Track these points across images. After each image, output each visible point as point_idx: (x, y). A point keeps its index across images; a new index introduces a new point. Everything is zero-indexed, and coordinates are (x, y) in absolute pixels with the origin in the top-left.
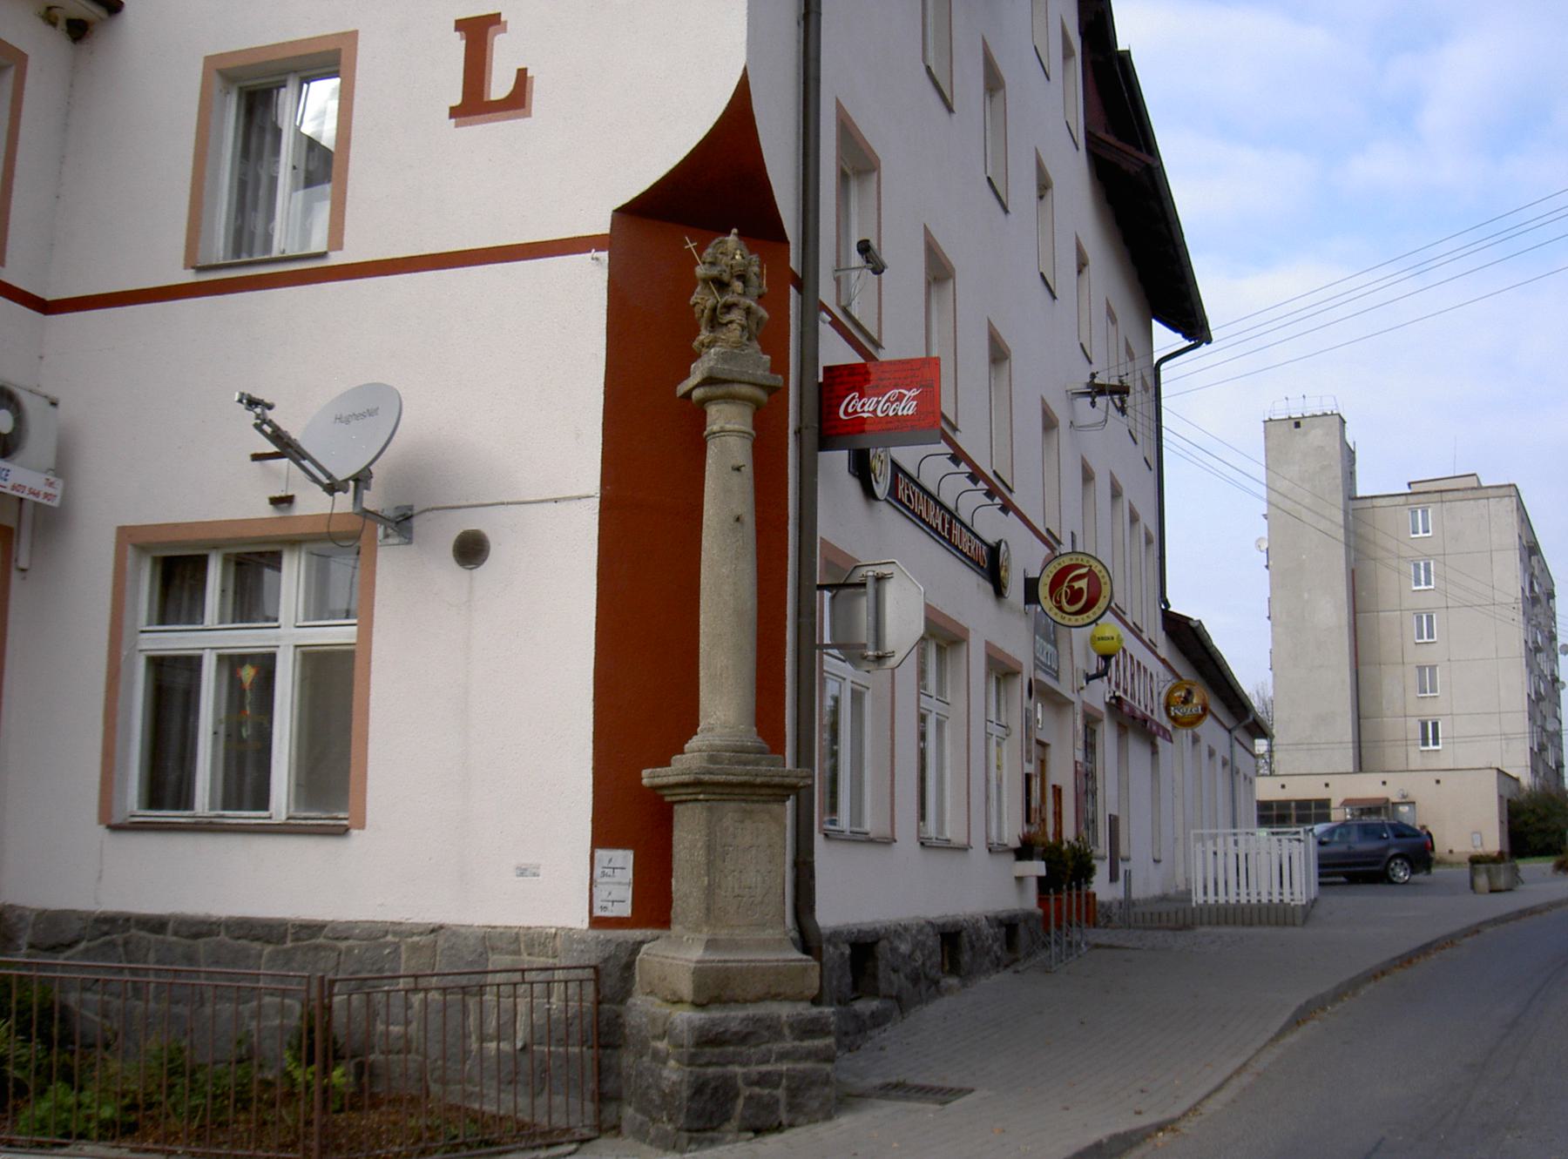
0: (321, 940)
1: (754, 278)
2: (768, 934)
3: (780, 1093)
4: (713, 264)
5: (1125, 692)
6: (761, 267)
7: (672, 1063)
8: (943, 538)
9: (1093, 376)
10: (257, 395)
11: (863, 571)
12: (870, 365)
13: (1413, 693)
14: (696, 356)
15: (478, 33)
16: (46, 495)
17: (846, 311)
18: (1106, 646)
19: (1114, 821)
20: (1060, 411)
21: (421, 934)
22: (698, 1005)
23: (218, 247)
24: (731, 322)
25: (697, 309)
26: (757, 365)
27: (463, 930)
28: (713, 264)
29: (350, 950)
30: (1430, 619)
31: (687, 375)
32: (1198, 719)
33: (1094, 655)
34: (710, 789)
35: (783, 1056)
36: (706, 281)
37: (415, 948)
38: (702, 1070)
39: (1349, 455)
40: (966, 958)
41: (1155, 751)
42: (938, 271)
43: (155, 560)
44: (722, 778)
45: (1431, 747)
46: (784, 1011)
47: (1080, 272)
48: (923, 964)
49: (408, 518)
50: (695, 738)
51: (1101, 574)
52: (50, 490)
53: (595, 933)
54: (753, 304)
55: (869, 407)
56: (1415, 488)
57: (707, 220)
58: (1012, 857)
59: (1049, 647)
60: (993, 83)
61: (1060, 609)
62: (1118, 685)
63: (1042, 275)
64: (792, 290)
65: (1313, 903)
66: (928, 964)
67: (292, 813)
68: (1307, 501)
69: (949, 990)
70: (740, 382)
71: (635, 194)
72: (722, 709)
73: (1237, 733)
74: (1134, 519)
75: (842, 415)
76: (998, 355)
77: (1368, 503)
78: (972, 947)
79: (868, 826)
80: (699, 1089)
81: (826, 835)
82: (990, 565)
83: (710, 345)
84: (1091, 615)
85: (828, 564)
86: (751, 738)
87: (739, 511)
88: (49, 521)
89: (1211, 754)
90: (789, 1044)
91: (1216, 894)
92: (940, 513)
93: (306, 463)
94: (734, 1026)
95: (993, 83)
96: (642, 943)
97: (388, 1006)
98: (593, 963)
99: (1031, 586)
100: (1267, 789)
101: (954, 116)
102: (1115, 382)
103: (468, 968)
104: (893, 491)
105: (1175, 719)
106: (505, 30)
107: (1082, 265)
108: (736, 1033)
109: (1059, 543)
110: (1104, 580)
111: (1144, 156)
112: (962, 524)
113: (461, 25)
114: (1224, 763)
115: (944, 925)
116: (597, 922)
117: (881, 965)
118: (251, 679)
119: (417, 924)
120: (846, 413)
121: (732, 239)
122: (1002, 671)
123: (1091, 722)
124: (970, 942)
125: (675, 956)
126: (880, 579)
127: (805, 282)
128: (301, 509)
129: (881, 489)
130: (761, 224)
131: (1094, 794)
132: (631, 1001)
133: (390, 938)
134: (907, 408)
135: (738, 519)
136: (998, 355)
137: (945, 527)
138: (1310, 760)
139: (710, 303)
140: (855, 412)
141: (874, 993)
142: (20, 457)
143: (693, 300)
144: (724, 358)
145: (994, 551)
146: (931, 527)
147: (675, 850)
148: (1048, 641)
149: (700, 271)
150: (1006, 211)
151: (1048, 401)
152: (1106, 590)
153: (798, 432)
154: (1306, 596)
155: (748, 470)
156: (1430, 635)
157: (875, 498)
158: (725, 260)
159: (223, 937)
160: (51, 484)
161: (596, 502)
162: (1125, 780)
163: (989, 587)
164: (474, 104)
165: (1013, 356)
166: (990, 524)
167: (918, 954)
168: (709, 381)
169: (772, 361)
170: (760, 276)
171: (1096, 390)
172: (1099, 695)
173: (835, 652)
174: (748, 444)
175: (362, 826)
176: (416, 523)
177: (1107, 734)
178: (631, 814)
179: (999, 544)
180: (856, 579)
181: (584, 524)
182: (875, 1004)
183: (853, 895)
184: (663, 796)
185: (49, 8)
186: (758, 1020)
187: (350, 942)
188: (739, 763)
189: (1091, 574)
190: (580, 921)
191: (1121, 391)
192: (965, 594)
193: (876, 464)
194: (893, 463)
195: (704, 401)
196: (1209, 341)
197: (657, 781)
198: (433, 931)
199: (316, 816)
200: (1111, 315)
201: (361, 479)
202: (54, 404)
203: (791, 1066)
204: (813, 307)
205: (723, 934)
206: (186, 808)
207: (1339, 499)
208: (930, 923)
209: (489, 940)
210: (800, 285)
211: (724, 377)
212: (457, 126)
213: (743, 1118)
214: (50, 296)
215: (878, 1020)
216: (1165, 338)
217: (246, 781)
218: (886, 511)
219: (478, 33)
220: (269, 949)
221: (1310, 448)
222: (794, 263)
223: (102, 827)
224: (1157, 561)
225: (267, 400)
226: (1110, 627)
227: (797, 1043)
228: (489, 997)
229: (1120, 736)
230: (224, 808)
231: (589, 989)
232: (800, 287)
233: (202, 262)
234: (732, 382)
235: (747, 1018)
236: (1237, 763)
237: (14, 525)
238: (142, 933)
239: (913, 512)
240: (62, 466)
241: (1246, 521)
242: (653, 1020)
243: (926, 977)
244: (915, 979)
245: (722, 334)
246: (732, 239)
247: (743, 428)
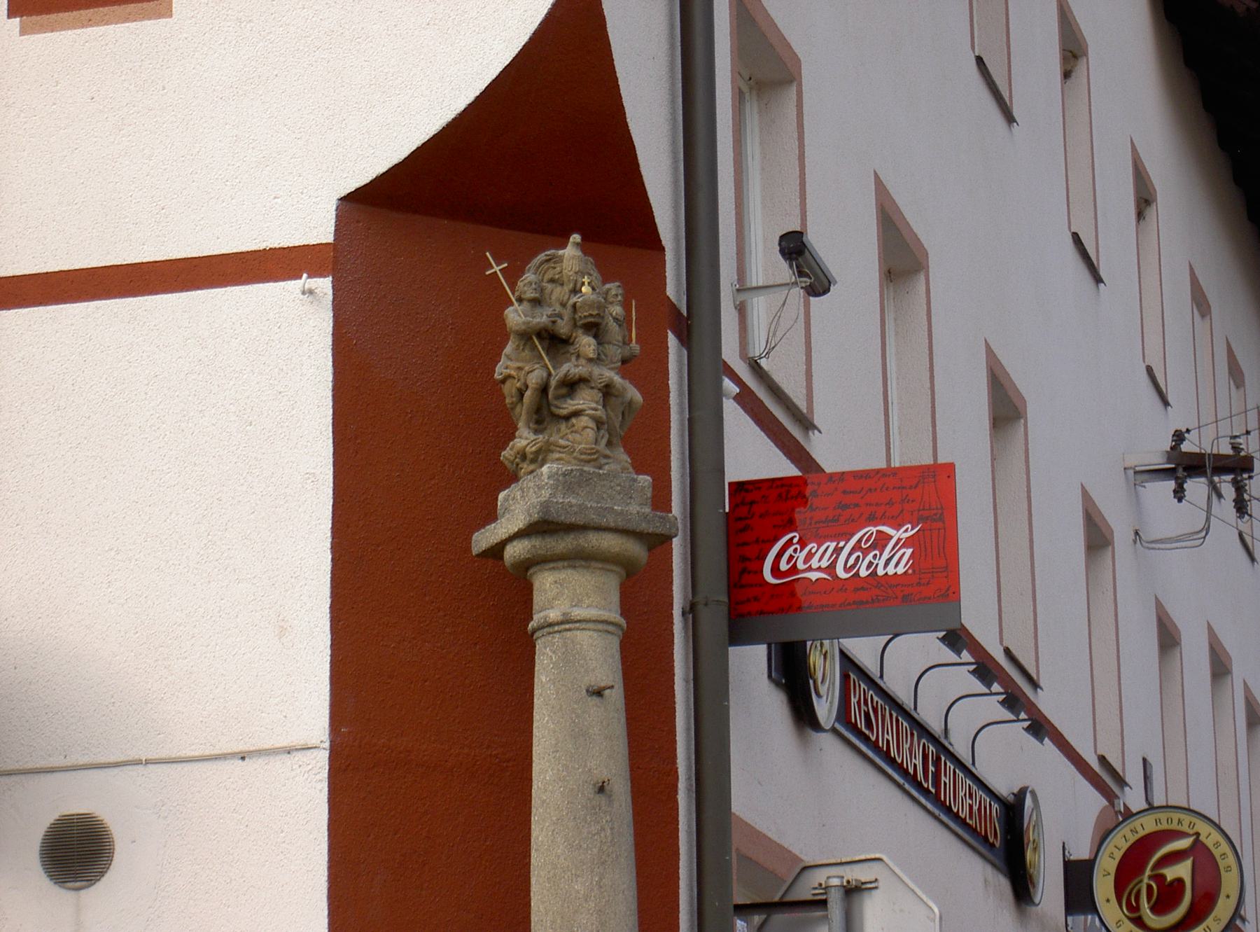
1: (613, 326)
4: (537, 302)
6: (626, 306)
8: (926, 792)
9: (1179, 437)
11: (820, 877)
12: (811, 478)
14: (511, 478)
17: (755, 367)
24: (577, 414)
25: (509, 389)
26: (623, 495)
28: (537, 302)
31: (490, 515)
36: (526, 336)
42: (901, 260)
47: (1140, 215)
51: (1220, 849)
54: (617, 379)
55: (814, 560)
63: (1076, 238)
64: (672, 340)
70: (599, 529)
71: (382, 168)
83: (539, 457)
87: (602, 773)
92: (919, 744)
99: (1078, 877)
102: (1226, 449)
104: (844, 713)
107: (1144, 202)
109: (1121, 782)
110: (1226, 861)
120: (775, 571)
121: (571, 253)
126: (852, 891)
127: (694, 325)
129: (825, 709)
130: (618, 222)
134: (895, 562)
135: (601, 790)
139: (535, 378)
143: (500, 370)
144: (567, 483)
146: (903, 771)
149: (516, 316)
150: (1010, 118)
151: (1094, 495)
152: (1229, 883)
153: (691, 610)
155: (616, 696)
157: (815, 725)
158: (558, 293)
161: (321, 759)
163: (1004, 884)
165: (1032, 411)
166: (1005, 758)
168: (541, 527)
170: (624, 322)
171: (1184, 466)
174: (615, 643)
179: (1021, 795)
180: (804, 891)
181: (300, 801)
189: (1199, 850)
191: (1237, 466)
193: (815, 659)
195: (527, 565)
200: (1200, 302)
204: (706, 371)
210: (685, 329)
212: (23, 32)
218: (828, 747)
222: (674, 288)
232: (685, 339)
239: (875, 746)
245: (560, 435)
246: (571, 253)
247: (605, 615)
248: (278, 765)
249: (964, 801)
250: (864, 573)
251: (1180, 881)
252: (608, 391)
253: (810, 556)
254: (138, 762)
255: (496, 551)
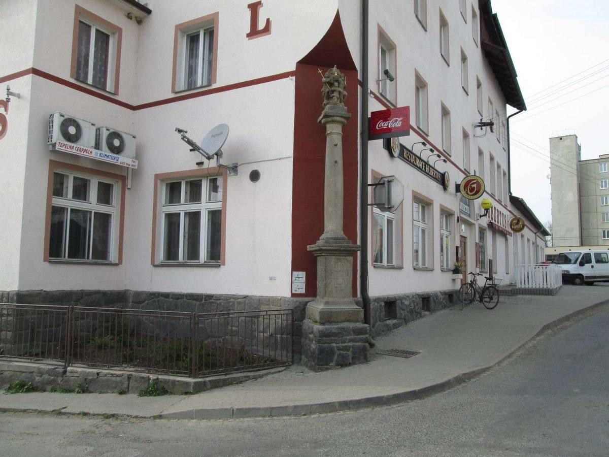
0: (212, 300)
2: (346, 300)
3: (350, 353)
4: (328, 77)
5: (495, 221)
7: (314, 342)
8: (423, 171)
9: (481, 120)
10: (181, 128)
13: (600, 222)
15: (254, 8)
16: (132, 165)
17: (381, 94)
18: (486, 206)
19: (490, 261)
20: (470, 132)
21: (241, 298)
22: (322, 324)
23: (182, 84)
24: (333, 96)
25: (323, 94)
27: (253, 297)
29: (221, 303)
30: (606, 198)
32: (521, 229)
33: (483, 210)
34: (325, 252)
35: (351, 341)
37: (239, 303)
38: (323, 345)
39: (579, 148)
40: (432, 305)
41: (506, 240)
43: (167, 184)
44: (328, 248)
45: (606, 238)
46: (351, 325)
47: (478, 88)
48: (414, 307)
49: (236, 167)
50: (323, 235)
52: (134, 164)
53: (292, 299)
56: (601, 157)
57: (328, 65)
58: (452, 272)
59: (466, 207)
60: (444, 23)
61: (467, 194)
62: (492, 219)
65: (561, 287)
66: (416, 308)
67: (206, 260)
68: (564, 162)
69: (425, 316)
72: (333, 225)
73: (538, 234)
74: (499, 167)
75: (377, 128)
76: (445, 112)
77: (585, 162)
78: (435, 302)
79: (394, 263)
80: (321, 351)
81: (374, 267)
82: (442, 180)
83: (327, 104)
84: (480, 194)
85: (374, 178)
86: (341, 234)
88: (137, 173)
89: (528, 240)
90: (352, 337)
91: (528, 284)
93: (201, 151)
94: (334, 331)
95: (444, 23)
96: (308, 302)
97: (232, 321)
98: (292, 308)
99: (458, 188)
100: (550, 251)
101: (428, 33)
102: (489, 121)
103: (252, 309)
105: (513, 230)
106: (263, 6)
108: (335, 333)
111: (502, 48)
112: (430, 166)
113: (250, 6)
114: (533, 243)
115: (423, 295)
116: (293, 295)
117: (397, 308)
118: (194, 217)
119: (240, 295)
120: (378, 127)
121: (335, 69)
122: (447, 214)
123: (482, 231)
124: (434, 300)
125: (317, 307)
126: (389, 182)
127: (364, 84)
128: (205, 166)
129: (396, 154)
130: (346, 64)
131: (484, 252)
132: (304, 321)
133: (232, 300)
134: (399, 124)
136: (445, 112)
137: (424, 168)
138: (565, 240)
139: (327, 90)
140: (381, 127)
141: (395, 318)
142: (123, 153)
145: (443, 175)
147: (317, 271)
148: (466, 204)
149: (324, 79)
150: (449, 65)
154: (563, 192)
156: (606, 203)
157: (394, 157)
159: (185, 299)
160: (134, 162)
161: (292, 160)
162: (496, 248)
163: (441, 187)
164: (254, 32)
166: (441, 167)
167: (412, 305)
169: (348, 109)
171: (482, 124)
172: (484, 222)
173: (375, 206)
174: (340, 137)
175: (224, 264)
176: (239, 168)
177: (489, 235)
178: (304, 260)
179: (445, 173)
180: (382, 182)
182: (395, 321)
183: (382, 284)
184: (314, 254)
185: (129, 14)
186: (343, 329)
187: (221, 301)
188: (336, 243)
189: (478, 183)
190: (288, 295)
191: (491, 124)
192: (431, 189)
194: (401, 145)
195: (326, 123)
196: (526, 110)
197: (311, 249)
198: (244, 297)
199: (213, 262)
201: (218, 154)
202: (134, 137)
203: (353, 344)
205: (330, 300)
206: (173, 259)
207: (575, 161)
208: (418, 295)
209: (261, 301)
211: (331, 114)
212: (249, 40)
213: (337, 361)
214: (135, 104)
215: (396, 326)
216: (511, 110)
217: (193, 252)
218: (399, 162)
219: (254, 8)
220: (198, 303)
221: (564, 146)
222: (359, 77)
223: (152, 266)
224: (508, 181)
225: (185, 130)
226: (485, 198)
227: (356, 336)
228: (261, 319)
229: (493, 235)
230: (188, 260)
231: (290, 317)
233: (177, 90)
234: (333, 116)
235: (338, 328)
236: (538, 243)
237: (126, 175)
238: (163, 298)
240: (138, 156)
241: (543, 167)
242: (309, 327)
243: (415, 311)
244: (411, 312)
246: (335, 69)
248: (285, 160)
249: (431, 172)
250: (393, 126)
251: (474, 187)
252: (340, 92)
253: (384, 124)
254: (264, 161)
255: (320, 121)
